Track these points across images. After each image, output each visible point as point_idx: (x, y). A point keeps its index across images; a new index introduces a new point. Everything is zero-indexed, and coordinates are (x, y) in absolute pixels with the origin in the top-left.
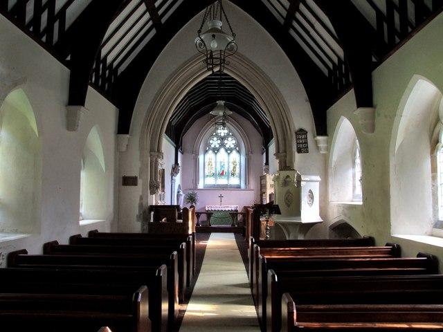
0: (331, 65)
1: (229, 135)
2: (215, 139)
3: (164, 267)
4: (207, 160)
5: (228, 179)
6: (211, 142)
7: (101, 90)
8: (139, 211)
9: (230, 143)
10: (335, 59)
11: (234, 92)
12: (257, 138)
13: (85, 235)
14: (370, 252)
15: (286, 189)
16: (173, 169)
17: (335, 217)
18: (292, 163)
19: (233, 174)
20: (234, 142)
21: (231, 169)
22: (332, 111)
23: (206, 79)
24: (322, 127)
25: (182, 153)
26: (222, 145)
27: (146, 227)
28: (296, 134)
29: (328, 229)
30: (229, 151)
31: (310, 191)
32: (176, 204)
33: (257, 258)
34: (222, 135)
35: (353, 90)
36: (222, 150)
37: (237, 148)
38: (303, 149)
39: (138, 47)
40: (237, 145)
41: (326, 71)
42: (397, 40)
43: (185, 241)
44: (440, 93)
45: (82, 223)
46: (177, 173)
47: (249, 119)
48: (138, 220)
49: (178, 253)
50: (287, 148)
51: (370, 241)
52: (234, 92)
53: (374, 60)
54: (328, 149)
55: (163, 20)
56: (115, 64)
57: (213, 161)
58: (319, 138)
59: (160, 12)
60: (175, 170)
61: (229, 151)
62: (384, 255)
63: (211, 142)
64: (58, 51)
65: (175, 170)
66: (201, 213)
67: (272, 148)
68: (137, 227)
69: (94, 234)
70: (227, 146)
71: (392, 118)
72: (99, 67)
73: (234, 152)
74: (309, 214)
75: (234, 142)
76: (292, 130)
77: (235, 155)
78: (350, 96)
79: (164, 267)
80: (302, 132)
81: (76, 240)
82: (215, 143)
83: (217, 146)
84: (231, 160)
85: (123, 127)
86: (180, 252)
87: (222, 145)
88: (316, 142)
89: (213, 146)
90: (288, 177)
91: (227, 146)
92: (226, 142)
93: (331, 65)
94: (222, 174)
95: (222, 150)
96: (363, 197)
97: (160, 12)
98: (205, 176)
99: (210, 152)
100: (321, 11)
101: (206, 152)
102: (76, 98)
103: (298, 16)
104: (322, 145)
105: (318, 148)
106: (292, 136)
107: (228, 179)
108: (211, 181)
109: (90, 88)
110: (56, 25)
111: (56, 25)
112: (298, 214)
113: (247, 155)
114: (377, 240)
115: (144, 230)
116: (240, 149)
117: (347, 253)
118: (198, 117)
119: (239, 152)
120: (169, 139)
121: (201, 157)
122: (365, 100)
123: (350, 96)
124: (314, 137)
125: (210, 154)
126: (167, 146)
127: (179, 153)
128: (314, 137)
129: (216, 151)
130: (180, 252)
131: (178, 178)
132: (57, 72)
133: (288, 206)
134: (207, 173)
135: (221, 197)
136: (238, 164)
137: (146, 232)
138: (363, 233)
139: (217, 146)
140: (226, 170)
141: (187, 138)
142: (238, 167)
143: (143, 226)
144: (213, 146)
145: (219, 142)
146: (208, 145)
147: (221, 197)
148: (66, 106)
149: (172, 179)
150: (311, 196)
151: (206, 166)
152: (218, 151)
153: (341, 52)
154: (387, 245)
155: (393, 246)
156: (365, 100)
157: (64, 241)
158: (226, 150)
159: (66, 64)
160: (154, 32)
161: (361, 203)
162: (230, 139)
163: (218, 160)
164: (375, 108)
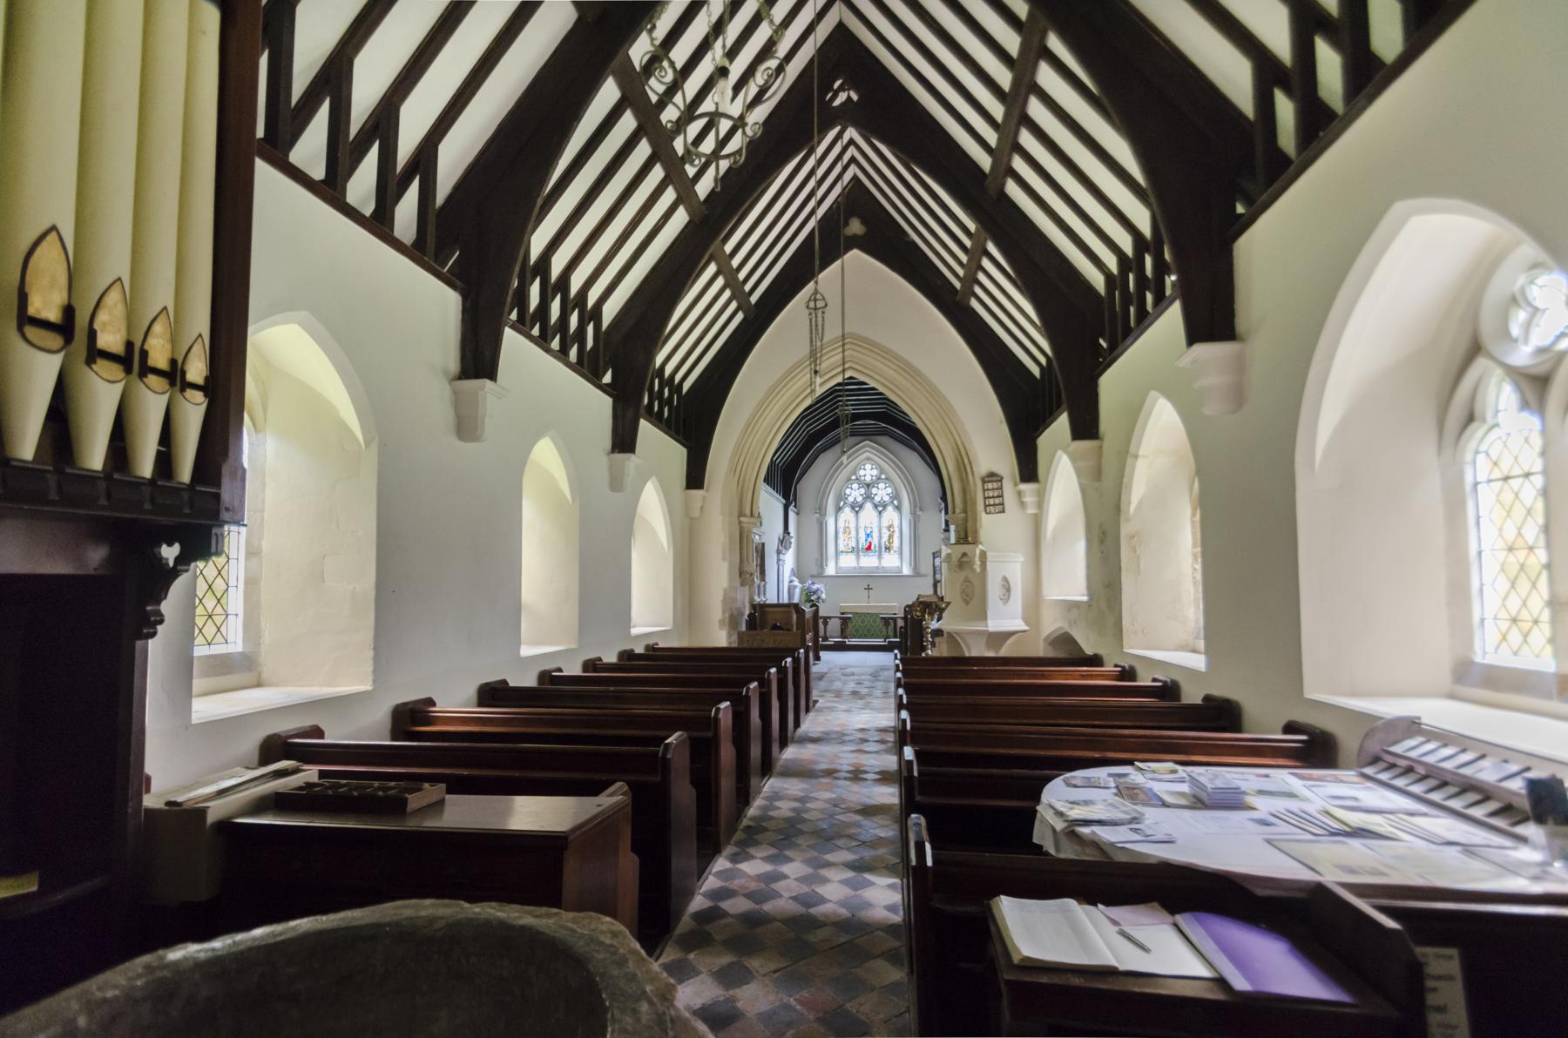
0: (1043, 361)
1: (879, 478)
2: (855, 486)
4: (841, 524)
5: (880, 557)
6: (848, 491)
7: (657, 420)
8: (724, 612)
9: (882, 492)
13: (639, 650)
14: (1083, 676)
15: (962, 575)
16: (781, 542)
17: (1051, 624)
18: (976, 532)
19: (888, 549)
20: (889, 490)
21: (885, 538)
24: (1029, 470)
26: (868, 497)
27: (735, 638)
28: (984, 481)
30: (880, 507)
31: (1005, 579)
34: (868, 479)
36: (869, 506)
37: (895, 502)
38: (853, 548)
40: (896, 496)
45: (635, 631)
46: (787, 549)
47: (914, 449)
48: (721, 629)
50: (969, 503)
51: (1096, 660)
54: (1041, 503)
55: (754, 299)
57: (852, 525)
58: (1024, 487)
59: (747, 288)
60: (783, 542)
61: (880, 507)
63: (848, 491)
64: (589, 368)
65: (783, 542)
66: (830, 618)
68: (720, 638)
69: (651, 648)
70: (877, 499)
71: (1125, 453)
72: (659, 407)
73: (890, 508)
74: (1006, 617)
75: (889, 490)
76: (976, 474)
77: (891, 515)
78: (1062, 422)
80: (992, 476)
81: (627, 656)
82: (855, 493)
83: (860, 499)
84: (885, 523)
85: (695, 478)
87: (868, 497)
88: (1020, 494)
89: (851, 499)
90: (964, 554)
91: (877, 499)
92: (874, 491)
94: (869, 548)
95: (869, 506)
97: (747, 288)
98: (837, 553)
99: (847, 510)
101: (839, 509)
102: (624, 441)
103: (981, 277)
105: (1022, 504)
106: (975, 485)
107: (880, 557)
108: (848, 562)
109: (644, 424)
110: (590, 329)
111: (590, 329)
112: (983, 616)
113: (913, 513)
114: (1106, 659)
115: (730, 643)
116: (900, 502)
117: (1043, 677)
118: (824, 449)
119: (898, 508)
120: (771, 490)
121: (831, 521)
122: (1086, 427)
123: (1062, 422)
124: (1016, 485)
125: (847, 513)
126: (770, 503)
127: (792, 515)
128: (1016, 485)
129: (857, 508)
130: (782, 671)
131: (789, 558)
132: (595, 406)
133: (967, 603)
134: (841, 547)
135: (868, 588)
136: (897, 529)
137: (735, 645)
138: (1089, 650)
139: (860, 499)
140: (875, 541)
141: (808, 485)
142: (896, 535)
143: (729, 635)
144: (851, 499)
145: (862, 491)
146: (841, 497)
147: (868, 588)
148: (608, 454)
149: (779, 560)
150: (1007, 589)
151: (841, 535)
152: (861, 507)
154: (1116, 666)
155: (1123, 667)
156: (1086, 427)
157: (611, 657)
158: (876, 506)
159: (603, 388)
160: (740, 316)
161: (1085, 598)
162: (882, 485)
163: (862, 525)
164: (1102, 440)
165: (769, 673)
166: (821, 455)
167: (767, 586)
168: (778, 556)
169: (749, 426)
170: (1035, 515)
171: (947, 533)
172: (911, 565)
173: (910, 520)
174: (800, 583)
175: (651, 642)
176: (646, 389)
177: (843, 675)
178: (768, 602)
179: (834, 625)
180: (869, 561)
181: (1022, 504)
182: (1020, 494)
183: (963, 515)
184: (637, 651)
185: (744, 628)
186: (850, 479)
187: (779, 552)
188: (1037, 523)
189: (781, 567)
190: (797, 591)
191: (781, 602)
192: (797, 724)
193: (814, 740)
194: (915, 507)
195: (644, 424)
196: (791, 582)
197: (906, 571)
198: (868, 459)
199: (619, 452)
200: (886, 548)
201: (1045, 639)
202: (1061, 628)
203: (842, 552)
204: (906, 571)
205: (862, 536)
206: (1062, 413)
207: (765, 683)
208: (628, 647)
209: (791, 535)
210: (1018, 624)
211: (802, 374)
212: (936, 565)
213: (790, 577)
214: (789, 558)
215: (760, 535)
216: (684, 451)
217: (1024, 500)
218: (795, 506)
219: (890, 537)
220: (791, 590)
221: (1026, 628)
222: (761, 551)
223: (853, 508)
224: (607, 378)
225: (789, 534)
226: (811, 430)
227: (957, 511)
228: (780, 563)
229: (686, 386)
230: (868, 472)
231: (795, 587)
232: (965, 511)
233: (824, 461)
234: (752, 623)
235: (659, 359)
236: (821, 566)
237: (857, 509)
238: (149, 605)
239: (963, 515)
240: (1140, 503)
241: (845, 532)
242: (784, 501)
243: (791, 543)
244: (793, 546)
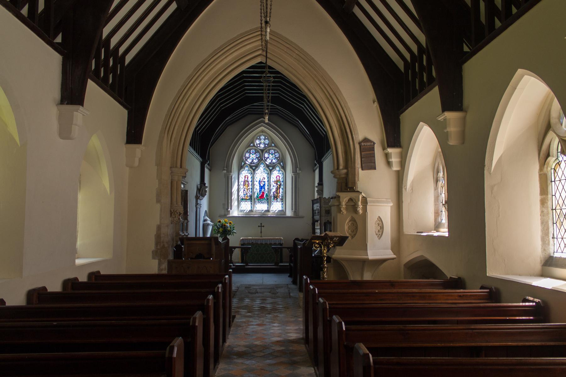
0: (408, 56)
3: (198, 315)
7: (103, 83)
10: (414, 48)
11: (279, 90)
12: (307, 150)
13: (83, 278)
14: (460, 296)
18: (354, 183)
19: (276, 197)
22: (407, 116)
23: (243, 72)
25: (210, 170)
27: (165, 265)
28: (360, 143)
29: (403, 267)
30: (270, 168)
31: (380, 219)
32: (201, 235)
33: (316, 304)
35: (436, 89)
39: (365, 7)
41: (401, 65)
42: (498, 24)
43: (221, 282)
44: (552, 93)
45: (78, 262)
46: (203, 196)
48: (154, 258)
49: (214, 297)
51: (458, 283)
52: (279, 90)
53: (466, 49)
54: (403, 163)
56: (122, 50)
57: (250, 179)
60: (201, 191)
61: (270, 168)
62: (483, 301)
65: (201, 191)
67: (327, 163)
69: (95, 276)
79: (198, 315)
82: (252, 157)
86: (216, 295)
87: (261, 159)
88: (387, 156)
89: (268, 161)
93: (408, 56)
94: (262, 197)
95: (262, 168)
96: (160, 274)
98: (240, 200)
100: (213, 2)
101: (241, 167)
104: (395, 160)
105: (389, 164)
108: (246, 206)
109: (91, 85)
119: (284, 168)
121: (234, 175)
124: (384, 149)
125: (245, 173)
127: (207, 171)
129: (254, 168)
130: (216, 295)
131: (204, 203)
134: (241, 194)
137: (165, 272)
141: (217, 148)
143: (160, 264)
149: (197, 204)
153: (422, 38)
154: (482, 288)
155: (490, 289)
157: (55, 286)
158: (268, 166)
164: (466, 112)
165: (209, 299)
166: (228, 127)
167: (189, 223)
168: (197, 201)
169: (181, 94)
170: (398, 172)
171: (321, 186)
172: (292, 210)
173: (292, 177)
174: (211, 221)
175: (94, 269)
176: (93, 56)
177: (249, 293)
178: (189, 236)
179: (236, 255)
180: (261, 207)
181: (389, 164)
182: (387, 156)
183: (345, 171)
184: (81, 280)
185: (171, 257)
186: (249, 146)
187: (197, 198)
188: (400, 177)
189: (198, 209)
190: (210, 228)
191: (198, 236)
192: (224, 341)
193: (241, 355)
194: (296, 167)
195: (91, 85)
196: (205, 220)
197: (289, 213)
198: (263, 131)
199: (67, 104)
200: (274, 197)
201: (405, 265)
202: (422, 256)
203: (242, 199)
204: (289, 213)
205: (257, 187)
206: (434, 86)
207: (205, 309)
208: (72, 276)
209: (206, 185)
210: (389, 254)
211: (224, 56)
212: (315, 208)
213: (204, 217)
214: (204, 203)
215: (184, 184)
216: (126, 112)
217: (390, 160)
218: (209, 164)
219: (278, 189)
220: (205, 227)
221: (395, 256)
222: (185, 194)
223: (251, 167)
224: (59, 39)
225: (205, 184)
226: (223, 106)
227: (341, 167)
228: (198, 206)
229: (129, 58)
230: (261, 143)
231: (208, 224)
232: (346, 167)
233: (230, 131)
234: (178, 253)
235: (106, 31)
236: (78, 258)
237: (254, 168)
238: (312, 285)
239: (345, 171)
240: (413, 182)
241: (244, 184)
242: (201, 160)
243: (206, 191)
244: (207, 193)
